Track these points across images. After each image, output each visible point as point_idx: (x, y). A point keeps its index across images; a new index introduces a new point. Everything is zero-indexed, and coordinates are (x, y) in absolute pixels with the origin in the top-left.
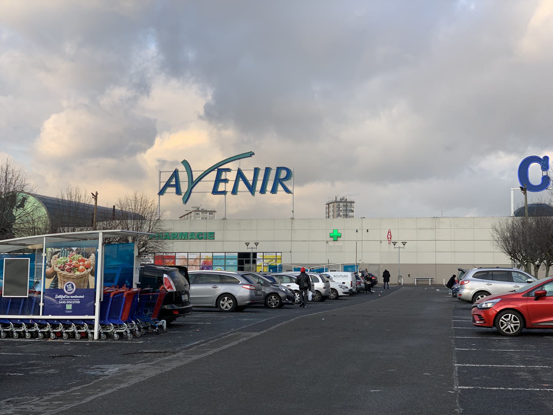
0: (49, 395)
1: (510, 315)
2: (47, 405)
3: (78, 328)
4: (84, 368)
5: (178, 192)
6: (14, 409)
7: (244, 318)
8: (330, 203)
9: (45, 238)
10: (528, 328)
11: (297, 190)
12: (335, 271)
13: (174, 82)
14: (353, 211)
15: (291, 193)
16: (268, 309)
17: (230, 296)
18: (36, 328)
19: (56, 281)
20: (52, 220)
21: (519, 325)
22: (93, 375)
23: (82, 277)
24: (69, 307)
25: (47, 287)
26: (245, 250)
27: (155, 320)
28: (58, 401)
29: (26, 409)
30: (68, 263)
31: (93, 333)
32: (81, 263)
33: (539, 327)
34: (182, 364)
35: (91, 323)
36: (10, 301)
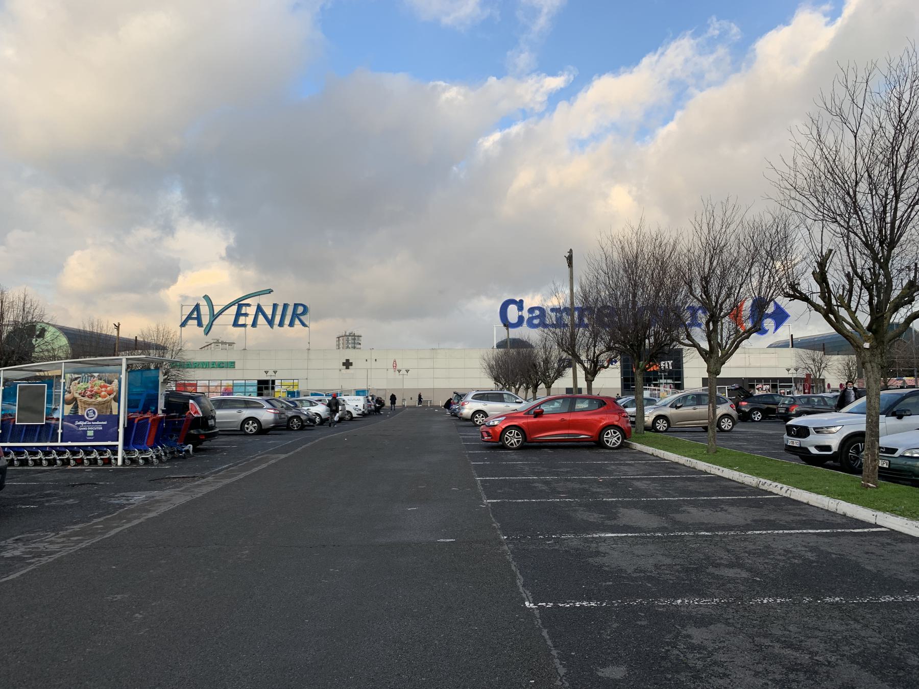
0: (67, 529)
1: (513, 431)
2: (63, 542)
3: (100, 455)
4: (108, 497)
5: (200, 324)
6: (23, 549)
7: (271, 440)
8: (341, 337)
9: (63, 363)
10: (527, 442)
11: (313, 325)
12: (348, 395)
13: (198, 225)
14: (360, 344)
15: (307, 326)
16: (291, 432)
17: (254, 420)
18: (54, 455)
19: (76, 408)
20: (73, 350)
21: (521, 439)
22: (118, 504)
23: (104, 403)
24: (90, 433)
25: (66, 413)
26: (264, 377)
27: (181, 445)
28: (77, 536)
29: (38, 548)
30: (89, 389)
31: (116, 459)
32: (103, 389)
33: (539, 441)
34: (213, 489)
35: (114, 450)
36: (25, 428)
